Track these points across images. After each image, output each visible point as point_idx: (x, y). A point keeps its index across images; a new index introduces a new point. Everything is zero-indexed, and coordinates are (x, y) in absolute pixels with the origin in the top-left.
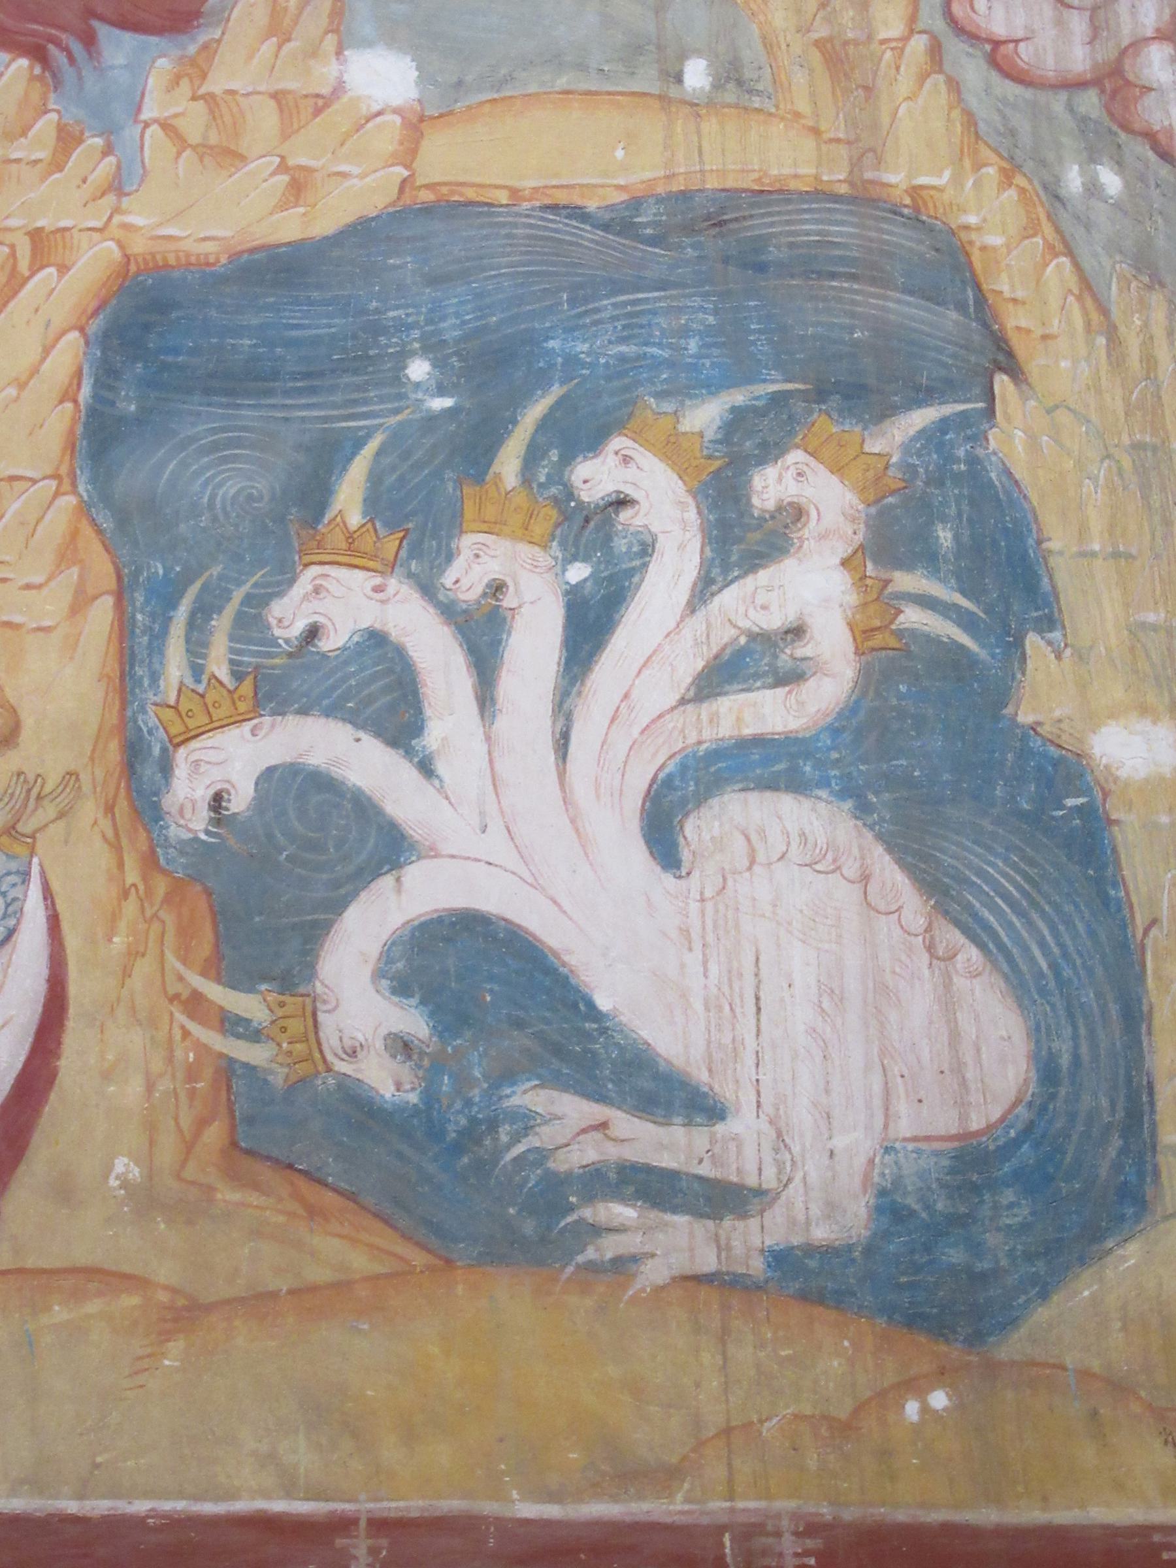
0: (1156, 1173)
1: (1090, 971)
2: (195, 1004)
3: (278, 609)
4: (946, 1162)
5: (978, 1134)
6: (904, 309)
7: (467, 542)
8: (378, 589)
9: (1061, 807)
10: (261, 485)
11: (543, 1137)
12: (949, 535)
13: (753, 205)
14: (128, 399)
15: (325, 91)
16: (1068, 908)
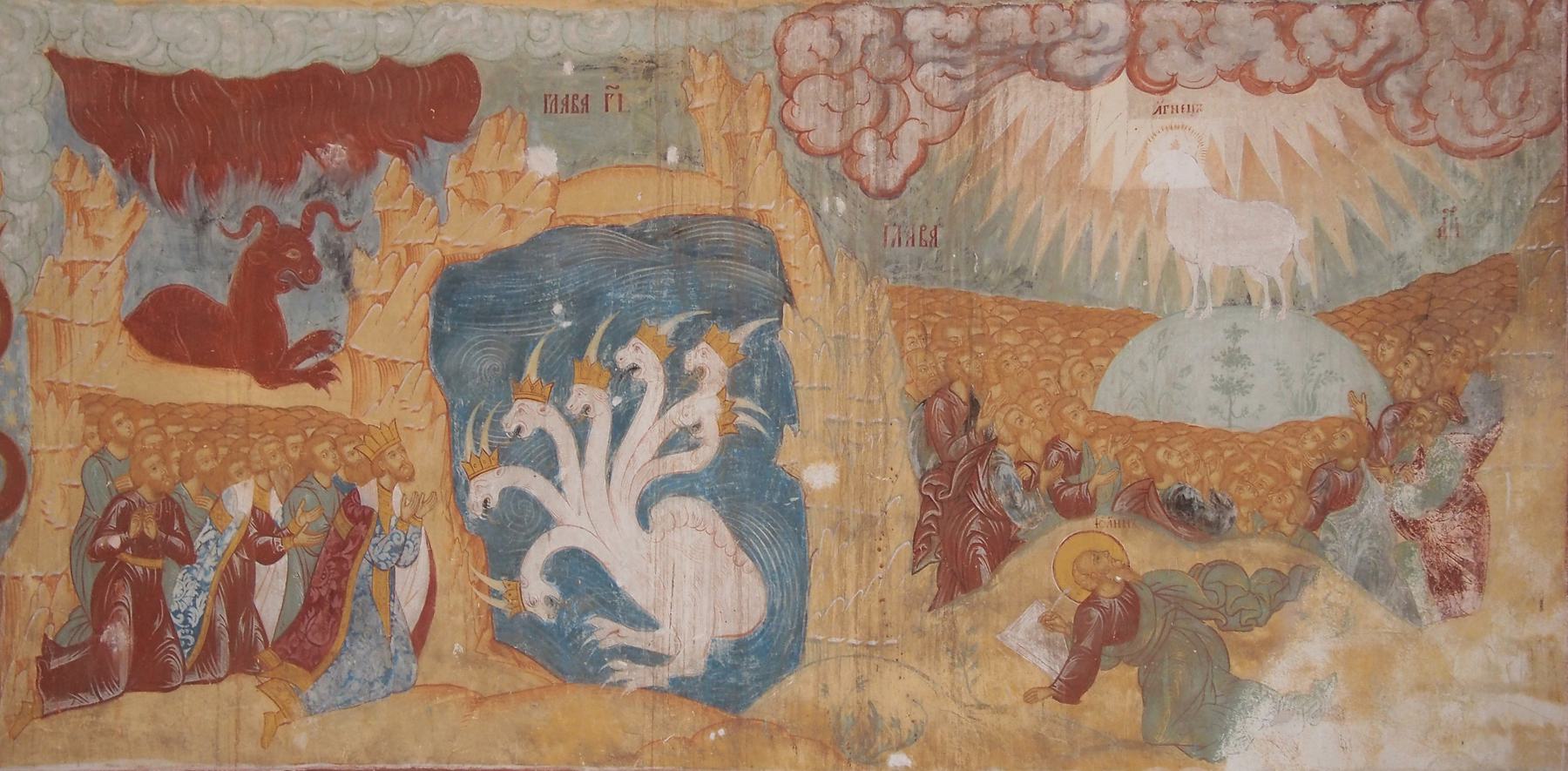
2: (479, 585)
7: (575, 388)
11: (598, 636)
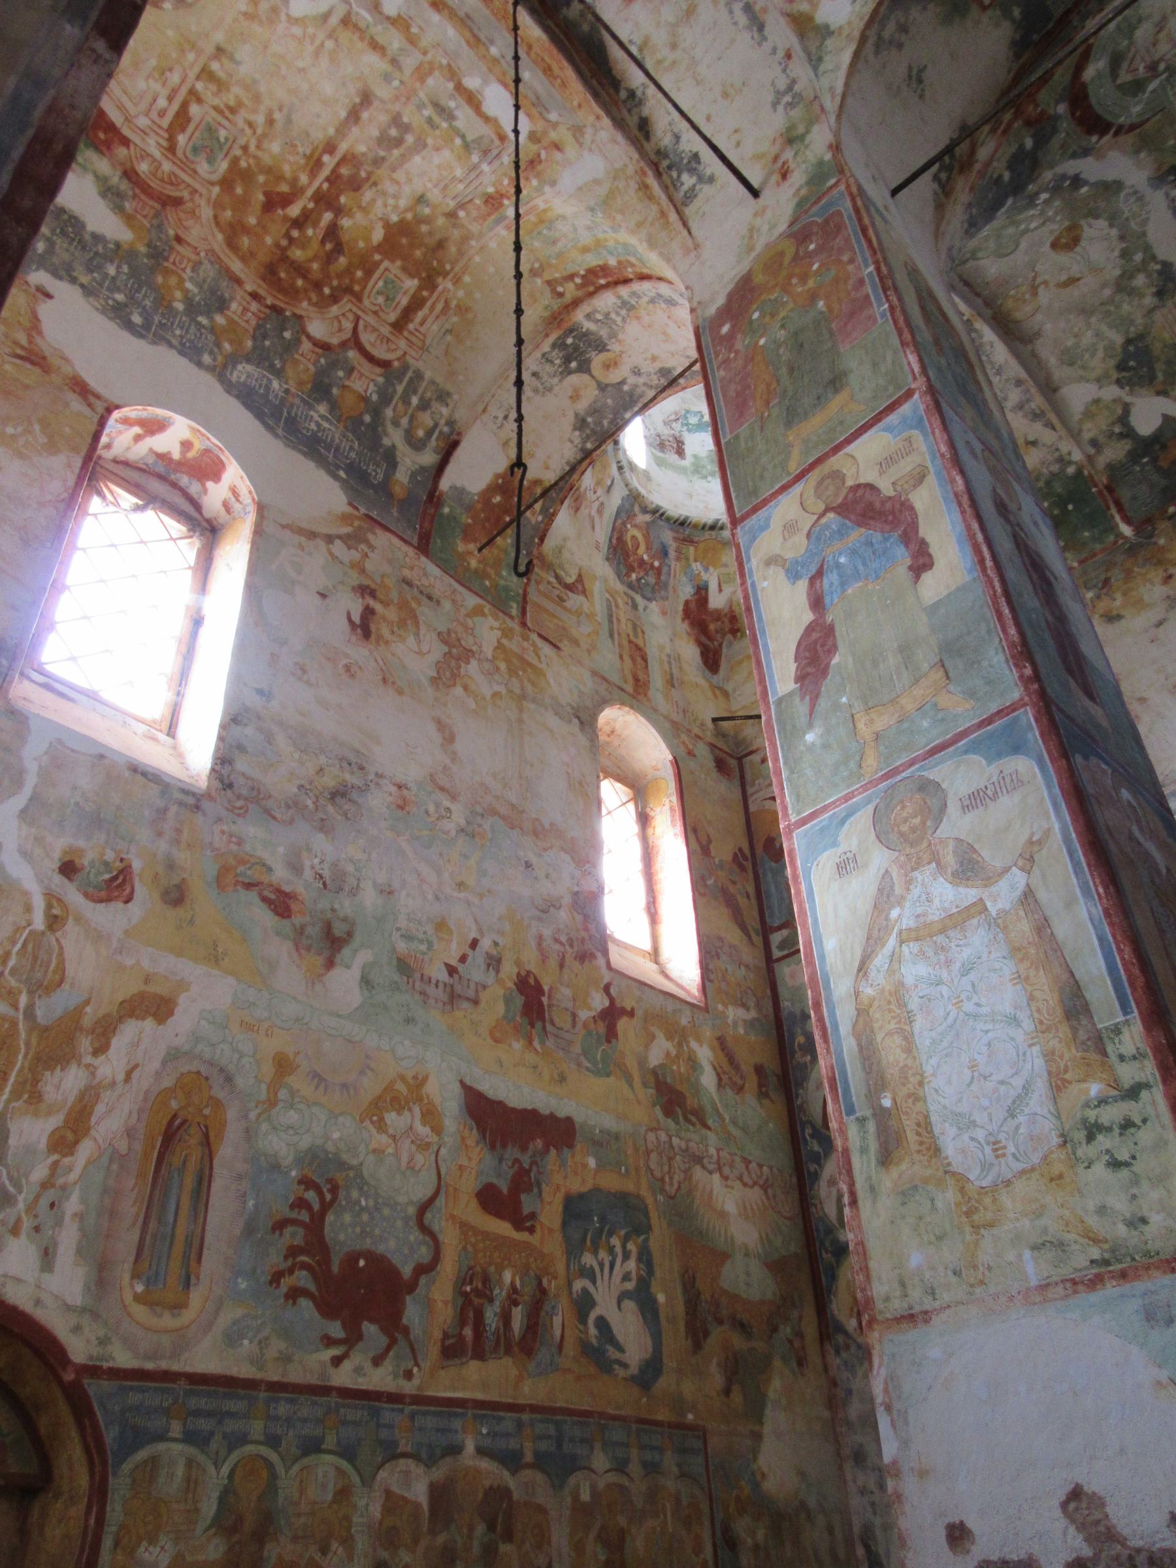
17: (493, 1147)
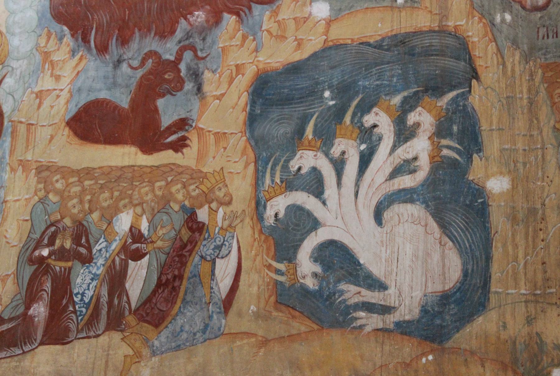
0: (489, 299)
1: (479, 246)
2: (269, 267)
3: (292, 163)
4: (438, 298)
5: (447, 291)
6: (450, 63)
7: (337, 141)
8: (315, 156)
9: (477, 202)
10: (289, 130)
12: (456, 128)
13: (413, 36)
14: (258, 109)
15: (307, 16)
16: (475, 230)
17: (103, 49)
